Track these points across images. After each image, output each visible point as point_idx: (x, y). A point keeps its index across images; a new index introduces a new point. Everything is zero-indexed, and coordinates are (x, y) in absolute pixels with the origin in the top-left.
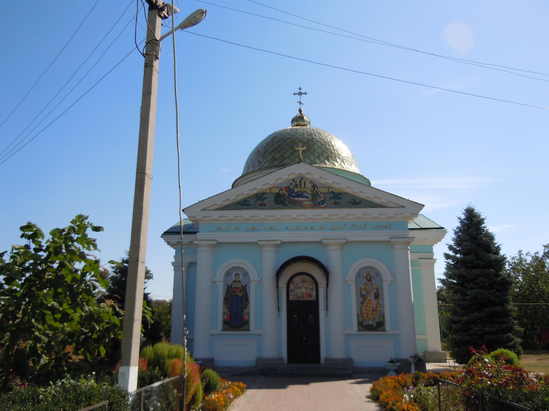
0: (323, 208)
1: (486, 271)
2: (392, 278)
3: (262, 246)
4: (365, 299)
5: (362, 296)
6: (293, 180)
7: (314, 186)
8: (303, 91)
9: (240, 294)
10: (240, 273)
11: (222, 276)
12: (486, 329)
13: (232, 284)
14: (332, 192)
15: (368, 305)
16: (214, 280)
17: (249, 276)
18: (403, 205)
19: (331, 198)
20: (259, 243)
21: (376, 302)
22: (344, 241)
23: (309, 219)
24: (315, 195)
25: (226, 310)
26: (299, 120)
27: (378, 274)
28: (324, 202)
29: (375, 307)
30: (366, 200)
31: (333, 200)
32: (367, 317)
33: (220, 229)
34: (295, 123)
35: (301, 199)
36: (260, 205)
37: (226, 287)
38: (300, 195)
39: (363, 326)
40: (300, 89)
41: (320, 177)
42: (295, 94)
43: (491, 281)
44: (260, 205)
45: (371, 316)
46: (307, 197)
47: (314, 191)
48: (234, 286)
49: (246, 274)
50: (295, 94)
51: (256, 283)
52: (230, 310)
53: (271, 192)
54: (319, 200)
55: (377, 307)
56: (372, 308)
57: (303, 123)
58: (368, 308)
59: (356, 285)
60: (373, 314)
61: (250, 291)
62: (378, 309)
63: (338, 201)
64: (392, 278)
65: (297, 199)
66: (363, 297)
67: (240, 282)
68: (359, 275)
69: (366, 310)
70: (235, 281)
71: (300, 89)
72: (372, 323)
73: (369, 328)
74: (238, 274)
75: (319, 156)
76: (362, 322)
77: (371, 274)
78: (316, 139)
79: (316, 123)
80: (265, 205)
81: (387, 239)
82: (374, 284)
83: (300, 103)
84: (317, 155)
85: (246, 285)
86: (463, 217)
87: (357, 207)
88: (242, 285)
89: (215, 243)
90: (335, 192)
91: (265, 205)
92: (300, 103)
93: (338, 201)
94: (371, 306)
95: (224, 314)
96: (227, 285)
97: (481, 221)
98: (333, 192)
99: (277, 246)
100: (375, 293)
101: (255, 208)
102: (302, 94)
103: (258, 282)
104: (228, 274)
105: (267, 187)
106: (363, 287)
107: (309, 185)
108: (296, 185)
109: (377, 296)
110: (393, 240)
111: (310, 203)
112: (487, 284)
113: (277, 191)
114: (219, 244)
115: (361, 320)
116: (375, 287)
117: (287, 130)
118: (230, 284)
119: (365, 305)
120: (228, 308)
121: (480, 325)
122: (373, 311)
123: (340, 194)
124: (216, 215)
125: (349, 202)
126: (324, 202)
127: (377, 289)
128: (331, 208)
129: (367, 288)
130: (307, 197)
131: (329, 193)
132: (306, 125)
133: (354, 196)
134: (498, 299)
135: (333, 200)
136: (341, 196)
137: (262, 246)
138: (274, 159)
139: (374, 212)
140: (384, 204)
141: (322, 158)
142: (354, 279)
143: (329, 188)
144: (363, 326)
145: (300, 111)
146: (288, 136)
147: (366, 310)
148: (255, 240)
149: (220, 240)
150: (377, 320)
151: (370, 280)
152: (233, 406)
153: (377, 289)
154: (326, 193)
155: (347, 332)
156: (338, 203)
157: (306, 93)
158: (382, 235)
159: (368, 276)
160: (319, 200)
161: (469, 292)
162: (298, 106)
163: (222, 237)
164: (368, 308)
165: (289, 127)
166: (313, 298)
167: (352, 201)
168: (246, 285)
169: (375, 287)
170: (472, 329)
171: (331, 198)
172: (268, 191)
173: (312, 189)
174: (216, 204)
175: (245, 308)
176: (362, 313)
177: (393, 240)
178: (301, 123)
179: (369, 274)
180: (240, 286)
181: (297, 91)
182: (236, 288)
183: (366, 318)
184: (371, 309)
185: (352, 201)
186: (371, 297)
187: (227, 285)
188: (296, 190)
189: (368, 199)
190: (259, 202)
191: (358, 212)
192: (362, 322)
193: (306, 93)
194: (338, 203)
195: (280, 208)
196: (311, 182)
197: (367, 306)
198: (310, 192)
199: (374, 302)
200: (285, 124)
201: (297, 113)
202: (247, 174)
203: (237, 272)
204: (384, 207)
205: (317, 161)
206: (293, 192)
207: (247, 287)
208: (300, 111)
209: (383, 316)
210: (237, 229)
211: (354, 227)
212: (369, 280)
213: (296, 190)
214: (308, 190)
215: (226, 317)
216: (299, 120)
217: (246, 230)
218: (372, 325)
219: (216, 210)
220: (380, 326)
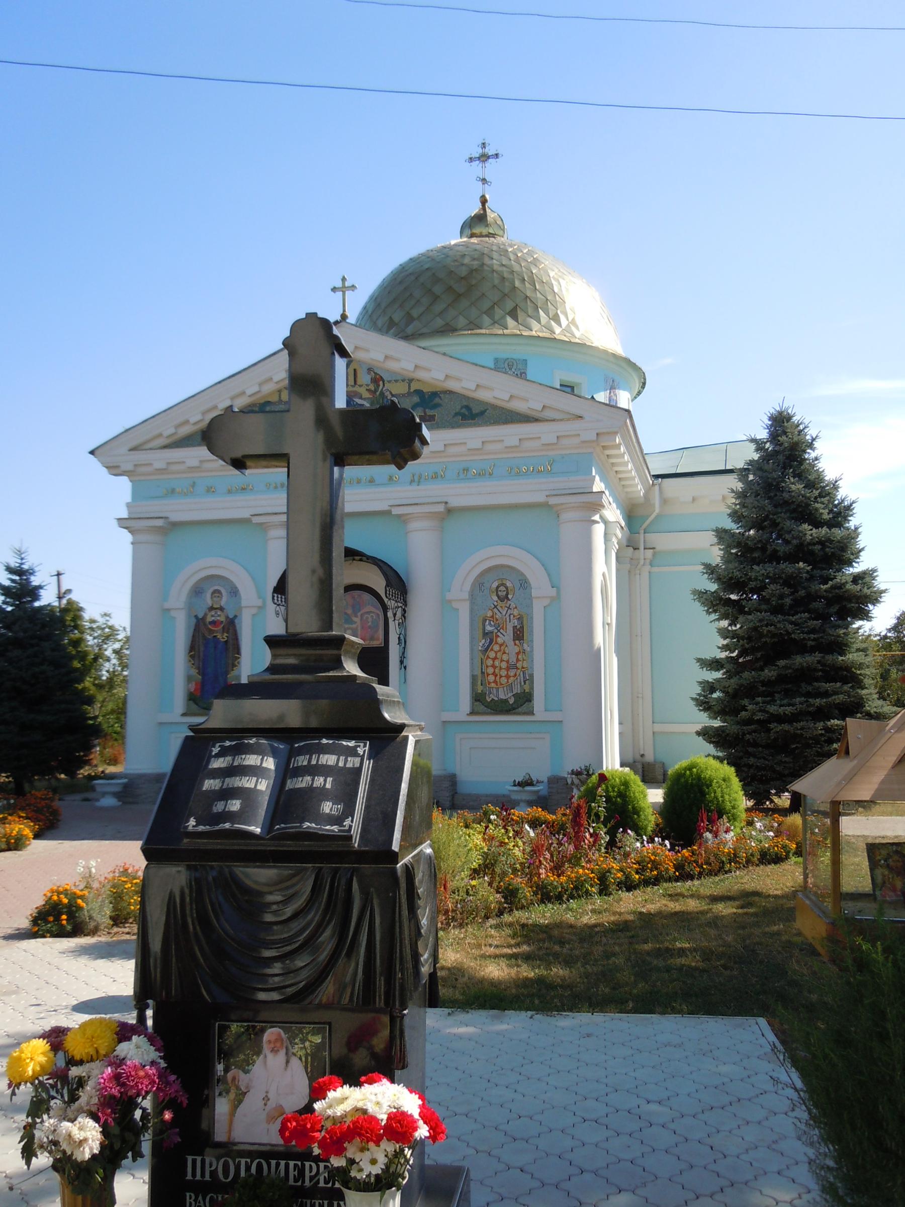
1: (787, 568)
2: (553, 592)
3: (403, 519)
4: (491, 643)
5: (485, 634)
7: (377, 379)
8: (490, 151)
9: (223, 637)
10: (223, 591)
11: (184, 597)
12: (772, 709)
13: (206, 615)
14: (418, 392)
15: (499, 655)
16: (167, 605)
17: (240, 596)
18: (579, 413)
20: (395, 511)
21: (517, 649)
23: (192, 469)
25: (194, 672)
26: (478, 221)
27: (524, 583)
29: (513, 660)
30: (495, 407)
32: (495, 682)
33: (173, 491)
34: (468, 232)
37: (194, 621)
39: (485, 703)
40: (484, 145)
41: (386, 357)
43: (802, 593)
45: (504, 680)
47: (376, 391)
48: (209, 619)
49: (234, 592)
51: (254, 611)
52: (202, 671)
55: (518, 660)
56: (508, 662)
57: (484, 231)
58: (497, 663)
59: (472, 611)
60: (508, 677)
61: (241, 627)
62: (519, 665)
63: (430, 412)
64: (553, 592)
66: (487, 638)
67: (221, 609)
68: (479, 584)
69: (493, 666)
70: (212, 608)
72: (503, 698)
73: (501, 708)
74: (219, 592)
75: (492, 307)
76: (483, 694)
77: (509, 584)
78: (491, 266)
81: (540, 498)
82: (513, 605)
83: (484, 181)
84: (486, 305)
85: (236, 616)
86: (763, 434)
87: (475, 425)
88: (227, 617)
89: (159, 523)
90: (426, 390)
92: (484, 181)
93: (430, 412)
94: (505, 657)
95: (189, 679)
96: (196, 616)
100: (515, 627)
102: (489, 157)
103: (259, 607)
104: (197, 591)
106: (490, 614)
109: (519, 635)
112: (788, 601)
114: (176, 525)
115: (480, 689)
116: (516, 612)
117: (450, 248)
118: (200, 616)
119: (492, 655)
120: (198, 668)
121: (759, 699)
122: (508, 669)
123: (435, 394)
124: (160, 459)
125: (456, 414)
129: (498, 616)
131: (409, 394)
132: (493, 235)
133: (468, 398)
134: (812, 636)
136: (437, 400)
137: (263, 527)
139: (510, 433)
140: (534, 414)
141: (498, 313)
142: (466, 596)
143: (411, 381)
144: (485, 703)
145: (484, 201)
146: (427, 266)
147: (493, 666)
148: (245, 514)
149: (175, 517)
150: (517, 690)
151: (507, 597)
152: (642, 756)
153: (520, 619)
154: (403, 395)
155: (446, 716)
158: (529, 491)
159: (502, 588)
162: (478, 190)
163: (463, 494)
164: (497, 663)
165: (455, 240)
166: (378, 642)
167: (464, 410)
168: (236, 616)
169: (516, 612)
170: (744, 708)
172: (275, 399)
173: (372, 387)
174: (160, 435)
175: (234, 666)
176: (483, 673)
177: (552, 501)
179: (503, 585)
180: (222, 619)
181: (477, 152)
182: (214, 623)
183: (493, 685)
184: (504, 665)
185: (464, 410)
186: (506, 637)
187: (196, 616)
189: (499, 403)
192: (483, 694)
193: (497, 155)
197: (496, 658)
198: (366, 395)
199: (512, 649)
200: (444, 234)
201: (476, 209)
203: (216, 588)
205: (486, 320)
207: (236, 621)
208: (484, 201)
209: (529, 679)
210: (210, 490)
215: (192, 686)
217: (230, 492)
218: (506, 701)
219: (165, 447)
220: (522, 702)
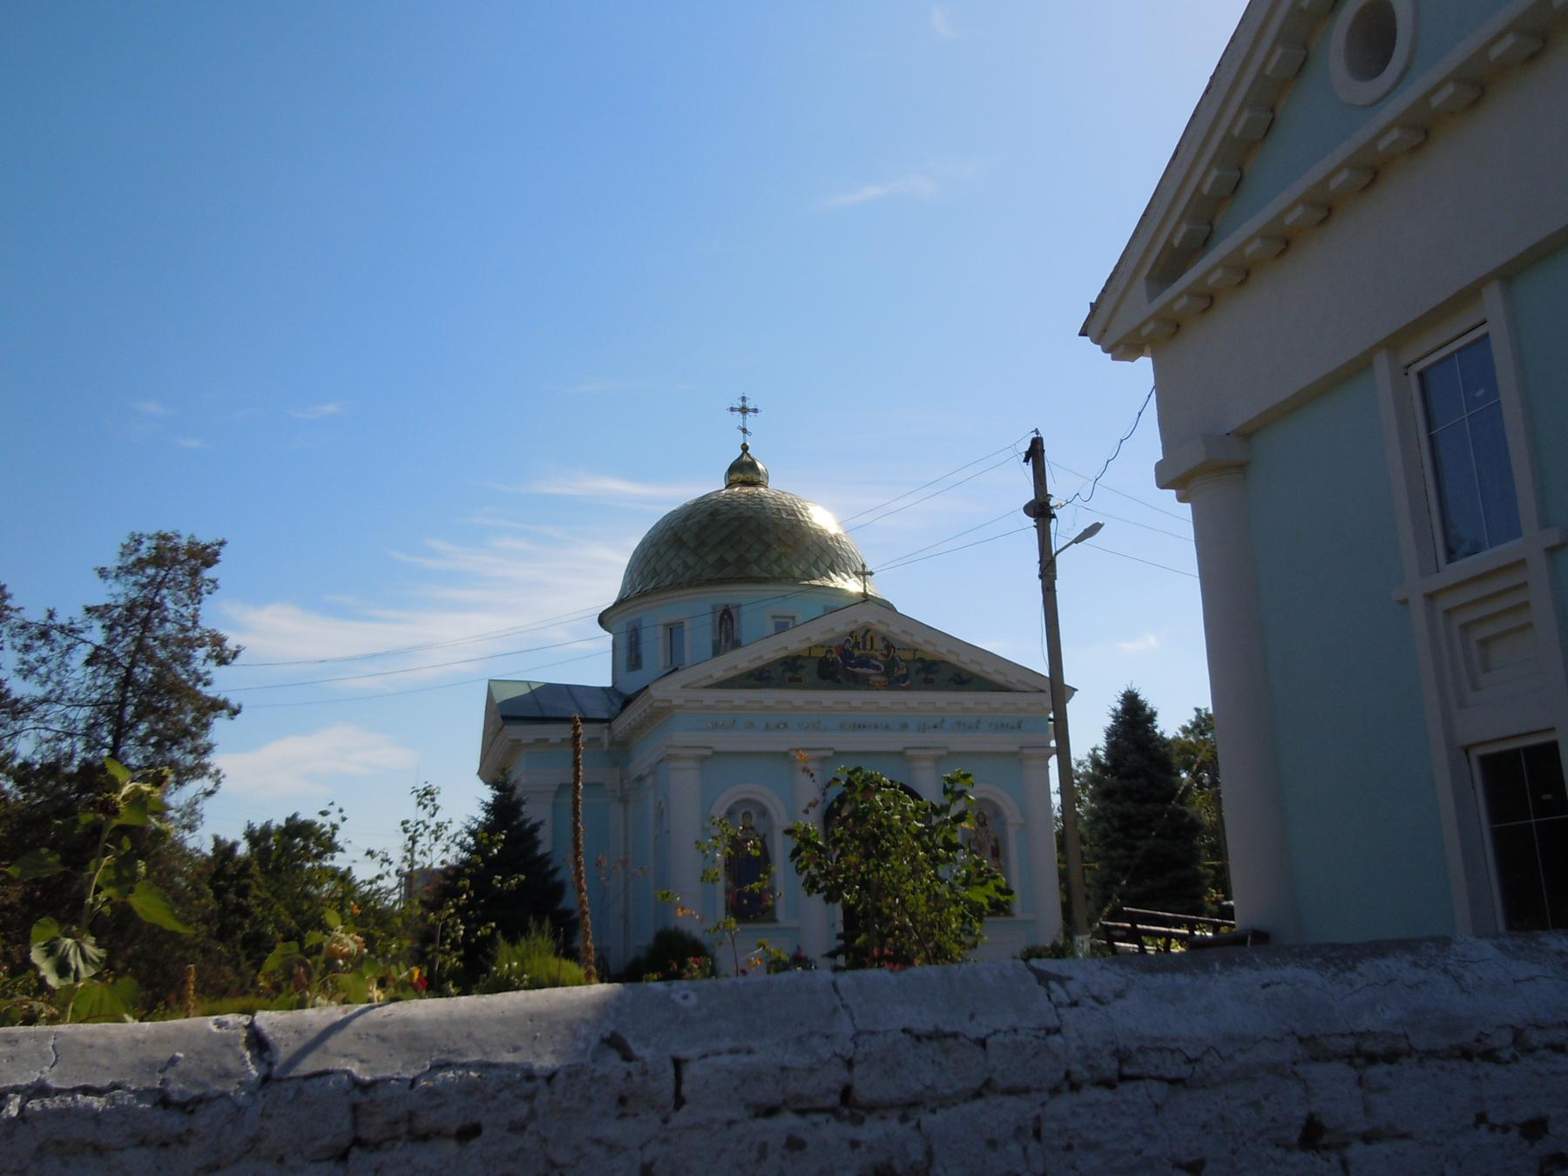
0: (904, 689)
6: (851, 634)
7: (889, 647)
19: (917, 672)
22: (944, 752)
24: (891, 664)
26: (744, 470)
27: (997, 812)
28: (905, 677)
30: (978, 677)
31: (923, 676)
35: (865, 670)
36: (791, 680)
38: (864, 662)
42: (732, 409)
44: (791, 680)
46: (877, 668)
49: (764, 812)
50: (732, 409)
53: (810, 657)
54: (897, 673)
65: (858, 670)
71: (744, 399)
75: (779, 558)
79: (782, 483)
80: (799, 680)
81: (1015, 748)
84: (812, 559)
91: (799, 680)
97: (1152, 716)
98: (921, 660)
99: (703, 759)
101: (781, 685)
105: (805, 645)
107: (879, 645)
108: (857, 645)
110: (1026, 751)
111: (883, 679)
113: (821, 653)
126: (905, 677)
127: (996, 840)
128: (918, 689)
130: (877, 668)
131: (915, 661)
135: (923, 676)
138: (723, 563)
145: (745, 448)
153: (996, 840)
156: (931, 681)
157: (755, 411)
160: (897, 673)
161: (1139, 844)
162: (739, 438)
171: (917, 672)
177: (1026, 751)
178: (749, 476)
181: (738, 404)
188: (857, 653)
190: (789, 674)
191: (968, 699)
193: (755, 411)
194: (931, 681)
195: (827, 688)
196: (884, 639)
200: (710, 483)
202: (643, 594)
204: (1008, 690)
206: (852, 657)
208: (745, 448)
210: (751, 726)
211: (960, 726)
212: (983, 824)
213: (857, 653)
214: (877, 654)
216: (744, 470)
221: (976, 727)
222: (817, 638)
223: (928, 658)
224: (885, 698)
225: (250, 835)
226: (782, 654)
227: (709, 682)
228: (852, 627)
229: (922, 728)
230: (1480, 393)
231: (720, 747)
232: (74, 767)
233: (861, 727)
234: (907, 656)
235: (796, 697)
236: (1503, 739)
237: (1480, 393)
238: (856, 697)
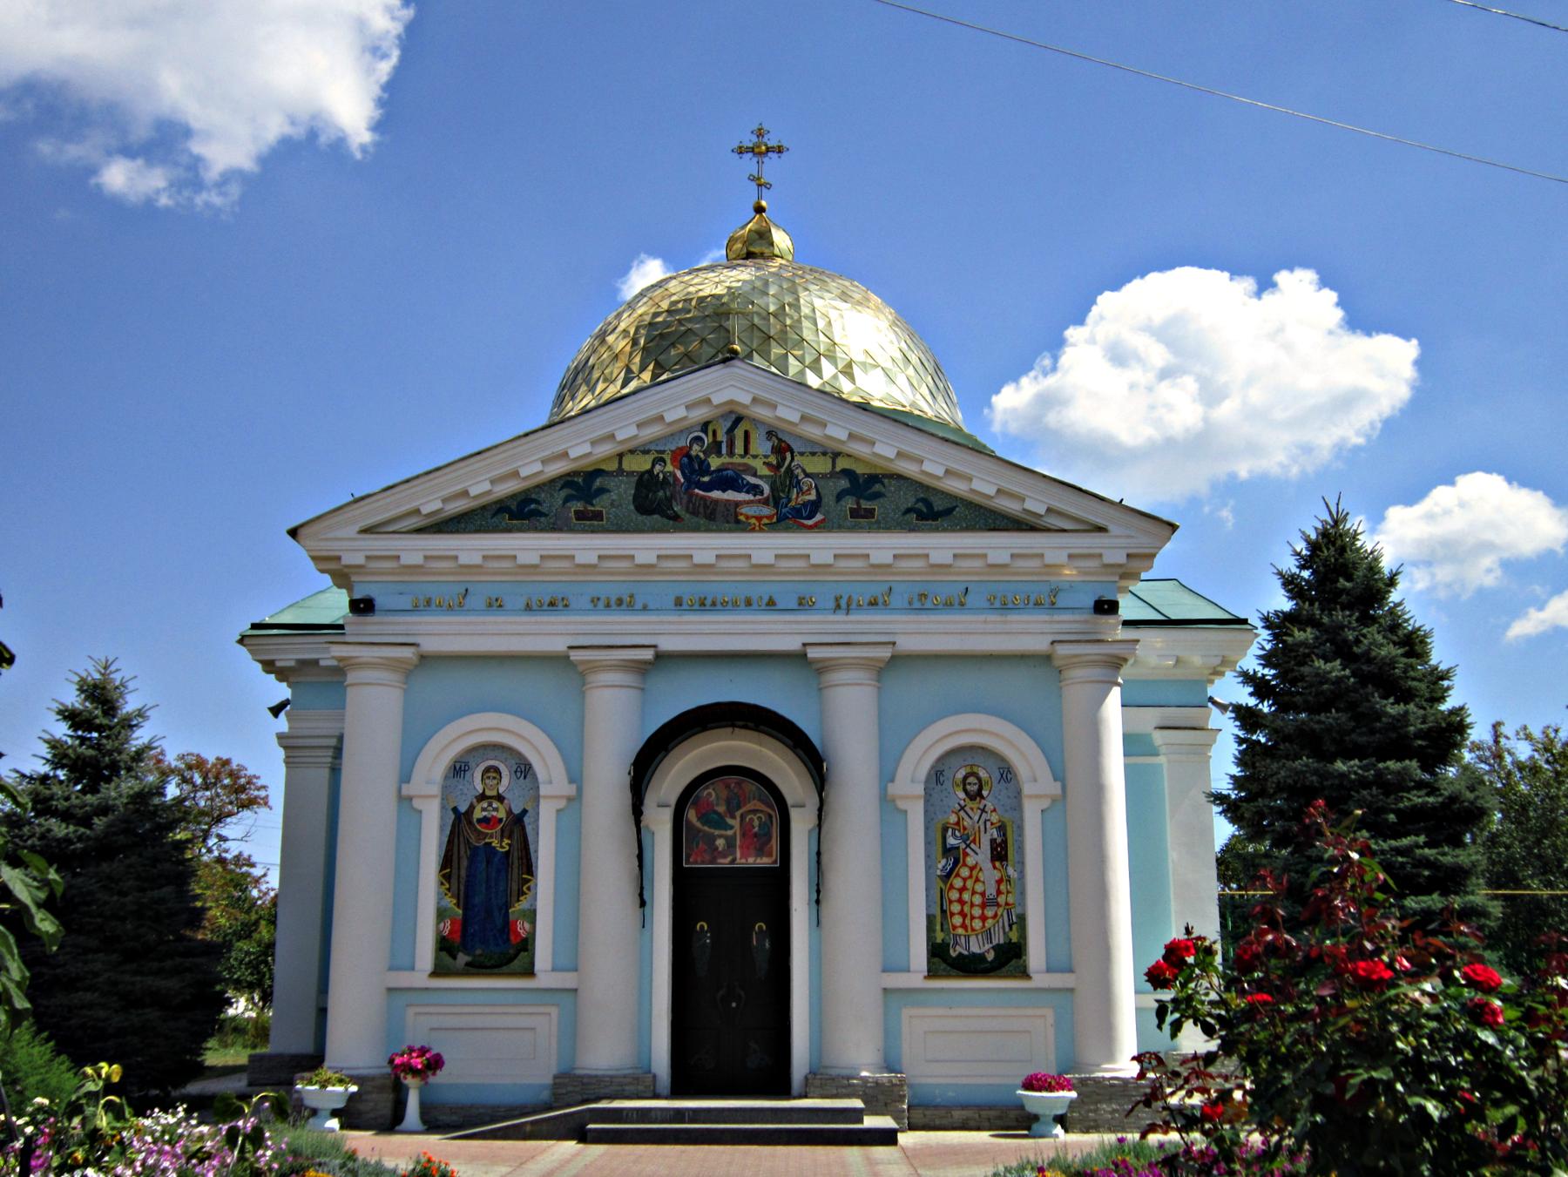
19: (840, 497)
24: (785, 480)
28: (814, 507)
31: (849, 503)
35: (731, 495)
36: (580, 516)
44: (580, 516)
54: (797, 498)
91: (598, 516)
98: (847, 473)
107: (760, 446)
111: (767, 511)
113: (642, 464)
126: (814, 507)
127: (1002, 828)
130: (755, 489)
131: (833, 474)
153: (1002, 828)
156: (870, 513)
171: (840, 497)
188: (715, 462)
190: (578, 505)
191: (940, 545)
194: (870, 513)
196: (771, 434)
204: (1033, 528)
206: (704, 468)
211: (922, 602)
213: (715, 462)
214: (758, 464)
221: (957, 603)
222: (627, 432)
223: (860, 470)
224: (764, 546)
225: (1459, 711)
226: (557, 469)
227: (414, 522)
228: (701, 414)
229: (841, 605)
230: (1369, 946)
231: (668, 644)
232: (1391, 700)
233: (704, 605)
234: (820, 466)
235: (585, 547)
236: (454, 740)
237: (1369, 946)
238: (704, 546)
